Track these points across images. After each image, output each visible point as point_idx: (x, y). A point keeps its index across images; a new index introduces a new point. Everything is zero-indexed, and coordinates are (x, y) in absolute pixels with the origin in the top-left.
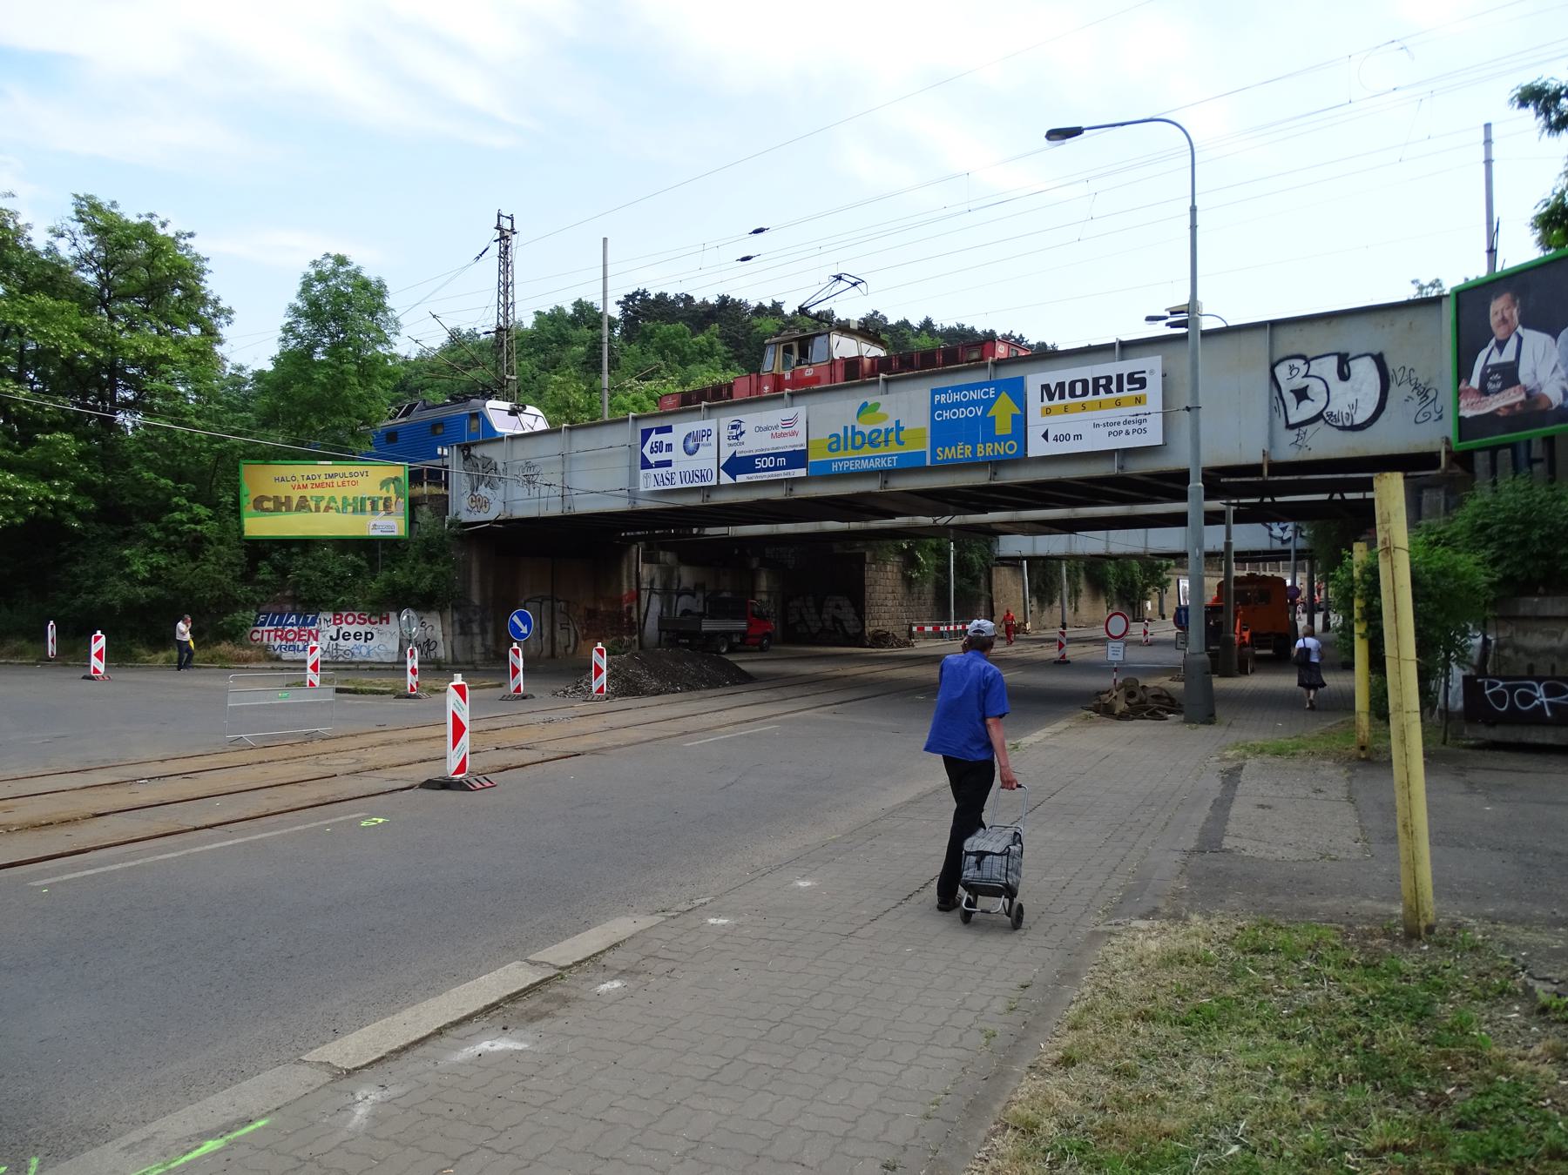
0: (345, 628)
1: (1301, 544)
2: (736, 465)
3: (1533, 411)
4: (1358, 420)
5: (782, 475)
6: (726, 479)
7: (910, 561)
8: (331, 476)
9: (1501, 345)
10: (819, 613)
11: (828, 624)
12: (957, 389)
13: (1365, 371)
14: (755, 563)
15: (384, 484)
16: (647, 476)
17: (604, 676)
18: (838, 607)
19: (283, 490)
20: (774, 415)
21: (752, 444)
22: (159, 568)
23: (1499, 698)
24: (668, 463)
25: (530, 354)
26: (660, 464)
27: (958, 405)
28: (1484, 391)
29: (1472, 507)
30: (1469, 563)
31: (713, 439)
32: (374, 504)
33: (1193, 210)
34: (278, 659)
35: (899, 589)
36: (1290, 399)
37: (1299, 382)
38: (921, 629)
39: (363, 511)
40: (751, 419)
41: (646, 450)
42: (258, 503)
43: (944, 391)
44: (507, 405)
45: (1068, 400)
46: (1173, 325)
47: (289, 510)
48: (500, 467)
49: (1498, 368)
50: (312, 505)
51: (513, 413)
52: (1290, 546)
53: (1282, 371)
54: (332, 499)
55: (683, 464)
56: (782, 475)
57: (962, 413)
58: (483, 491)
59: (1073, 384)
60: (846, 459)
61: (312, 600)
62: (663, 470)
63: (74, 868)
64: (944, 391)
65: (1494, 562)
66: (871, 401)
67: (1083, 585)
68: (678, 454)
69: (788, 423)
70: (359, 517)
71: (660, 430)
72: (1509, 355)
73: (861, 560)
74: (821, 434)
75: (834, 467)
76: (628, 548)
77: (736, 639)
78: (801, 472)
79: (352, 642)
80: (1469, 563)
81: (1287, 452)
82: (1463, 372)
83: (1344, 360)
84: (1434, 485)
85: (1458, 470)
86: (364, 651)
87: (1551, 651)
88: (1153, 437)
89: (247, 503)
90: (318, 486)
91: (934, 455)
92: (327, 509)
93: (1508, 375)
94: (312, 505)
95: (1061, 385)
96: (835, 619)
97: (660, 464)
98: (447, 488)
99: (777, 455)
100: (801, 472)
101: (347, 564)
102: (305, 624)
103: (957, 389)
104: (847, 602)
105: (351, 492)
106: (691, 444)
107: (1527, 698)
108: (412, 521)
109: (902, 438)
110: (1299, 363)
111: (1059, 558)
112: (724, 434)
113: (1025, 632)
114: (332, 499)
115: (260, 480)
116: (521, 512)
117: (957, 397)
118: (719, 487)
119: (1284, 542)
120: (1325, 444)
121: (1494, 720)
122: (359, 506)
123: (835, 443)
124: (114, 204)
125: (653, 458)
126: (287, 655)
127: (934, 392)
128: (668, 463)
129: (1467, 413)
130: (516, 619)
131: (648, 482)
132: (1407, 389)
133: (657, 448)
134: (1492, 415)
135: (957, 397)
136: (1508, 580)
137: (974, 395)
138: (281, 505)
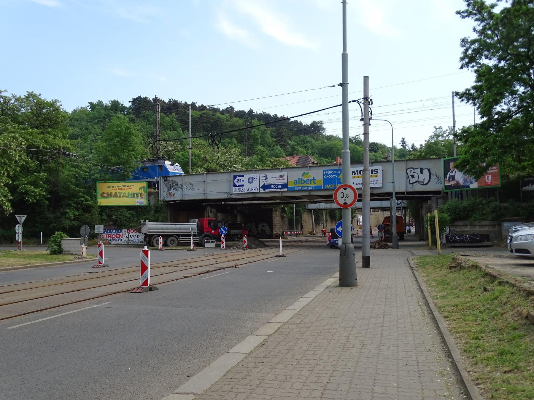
0: (131, 234)
1: (404, 205)
2: (265, 187)
3: (457, 186)
4: (425, 183)
5: (280, 190)
6: (262, 190)
7: (283, 211)
8: (124, 186)
9: (452, 172)
10: (257, 227)
11: (260, 231)
12: (330, 170)
13: (426, 172)
14: (235, 212)
15: (140, 189)
16: (235, 189)
17: (247, 243)
18: (263, 226)
19: (110, 191)
20: (277, 174)
21: (270, 182)
22: (76, 215)
23: (451, 238)
24: (243, 185)
25: (96, 123)
26: (240, 186)
27: (331, 174)
28: (449, 181)
29: (448, 203)
30: (446, 216)
31: (258, 179)
32: (137, 195)
33: (393, 140)
34: (110, 244)
35: (280, 220)
36: (410, 177)
37: (412, 174)
38: (286, 233)
39: (134, 197)
40: (270, 175)
41: (235, 181)
42: (102, 195)
43: (327, 171)
44: (170, 163)
45: (359, 175)
46: (383, 158)
47: (111, 197)
48: (179, 184)
49: (452, 176)
50: (119, 195)
51: (172, 165)
52: (400, 205)
53: (408, 171)
54: (125, 193)
55: (247, 185)
56: (280, 190)
57: (332, 176)
58: (172, 191)
59: (360, 171)
60: (299, 186)
61: (122, 225)
62: (241, 187)
63: (214, 274)
64: (327, 171)
65: (450, 216)
66: (306, 172)
67: (328, 218)
68: (246, 183)
69: (282, 176)
70: (133, 199)
71: (240, 176)
72: (453, 174)
73: (271, 211)
74: (292, 180)
75: (296, 189)
76: (206, 208)
77: (239, 236)
78: (286, 190)
79: (133, 238)
80: (446, 216)
81: (410, 190)
82: (445, 176)
83: (421, 169)
84: (440, 198)
85: (445, 195)
86: (137, 241)
87: (460, 231)
88: (380, 185)
89: (99, 194)
90: (120, 189)
91: (324, 187)
92: (123, 196)
93: (453, 178)
94: (119, 195)
95: (357, 171)
96: (262, 230)
97: (240, 186)
98: (158, 189)
99: (278, 185)
100: (286, 190)
101: (131, 214)
102: (118, 232)
103: (330, 170)
104: (267, 225)
105: (130, 191)
106: (251, 181)
107: (455, 238)
108: (148, 200)
109: (315, 181)
110: (412, 169)
111: (322, 209)
112: (261, 178)
113: (314, 234)
114: (125, 193)
115: (103, 187)
116: (187, 198)
117: (330, 172)
118: (260, 193)
119: (398, 204)
120: (418, 188)
121: (450, 242)
122: (133, 196)
123: (296, 182)
124: (40, 95)
125: (237, 184)
126: (113, 242)
127: (324, 171)
128: (243, 185)
129: (446, 185)
130: (222, 229)
131: (236, 190)
132: (435, 177)
133: (239, 181)
134: (451, 185)
135: (330, 172)
136: (453, 219)
137: (335, 172)
138: (109, 195)
